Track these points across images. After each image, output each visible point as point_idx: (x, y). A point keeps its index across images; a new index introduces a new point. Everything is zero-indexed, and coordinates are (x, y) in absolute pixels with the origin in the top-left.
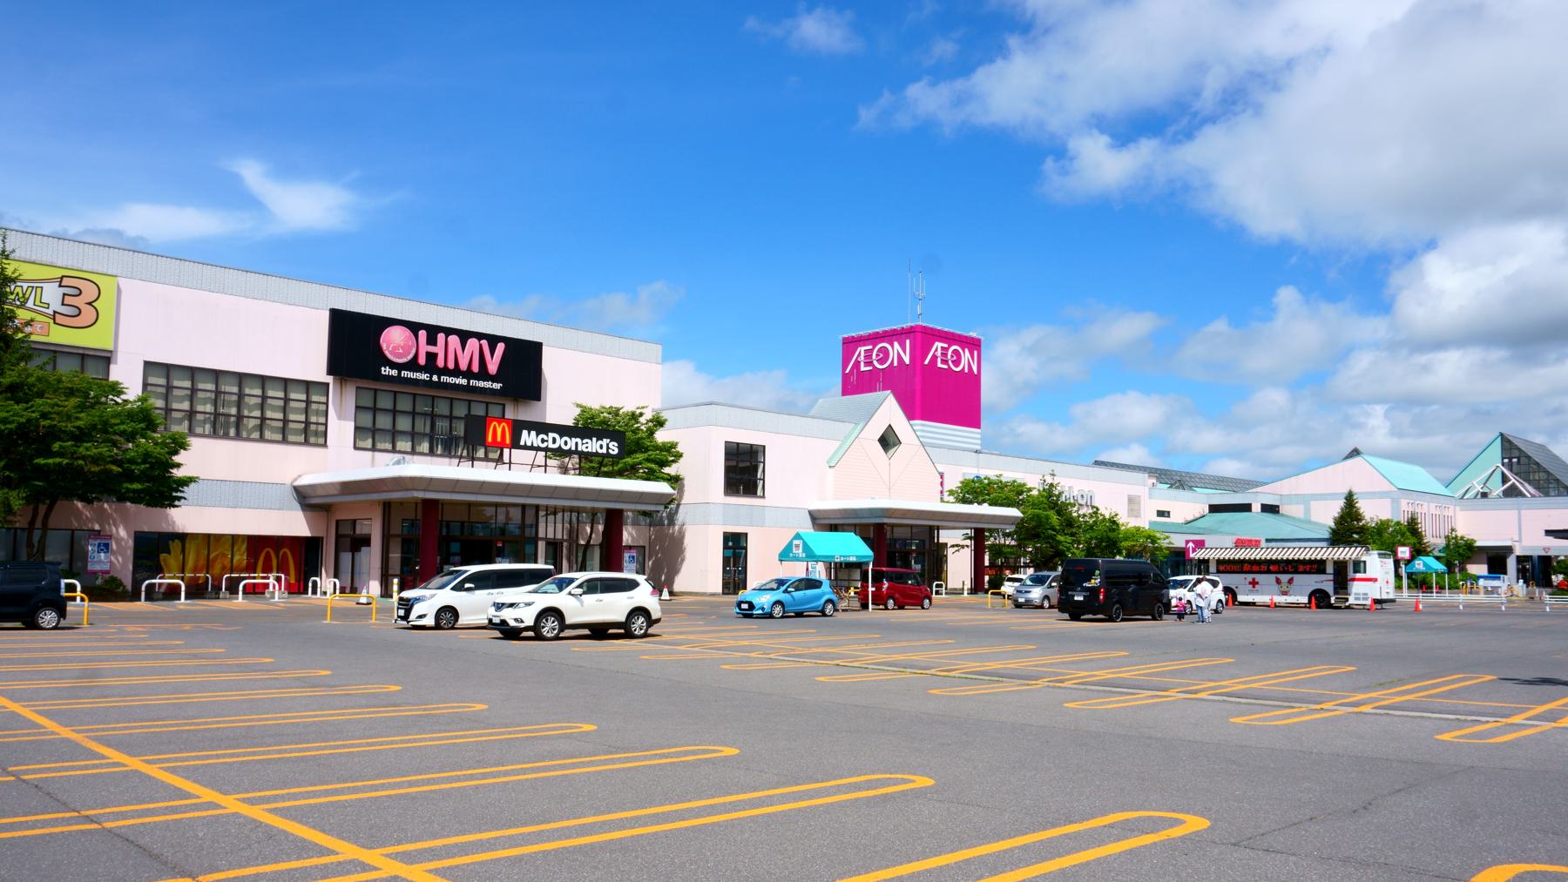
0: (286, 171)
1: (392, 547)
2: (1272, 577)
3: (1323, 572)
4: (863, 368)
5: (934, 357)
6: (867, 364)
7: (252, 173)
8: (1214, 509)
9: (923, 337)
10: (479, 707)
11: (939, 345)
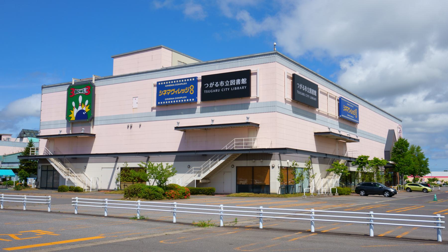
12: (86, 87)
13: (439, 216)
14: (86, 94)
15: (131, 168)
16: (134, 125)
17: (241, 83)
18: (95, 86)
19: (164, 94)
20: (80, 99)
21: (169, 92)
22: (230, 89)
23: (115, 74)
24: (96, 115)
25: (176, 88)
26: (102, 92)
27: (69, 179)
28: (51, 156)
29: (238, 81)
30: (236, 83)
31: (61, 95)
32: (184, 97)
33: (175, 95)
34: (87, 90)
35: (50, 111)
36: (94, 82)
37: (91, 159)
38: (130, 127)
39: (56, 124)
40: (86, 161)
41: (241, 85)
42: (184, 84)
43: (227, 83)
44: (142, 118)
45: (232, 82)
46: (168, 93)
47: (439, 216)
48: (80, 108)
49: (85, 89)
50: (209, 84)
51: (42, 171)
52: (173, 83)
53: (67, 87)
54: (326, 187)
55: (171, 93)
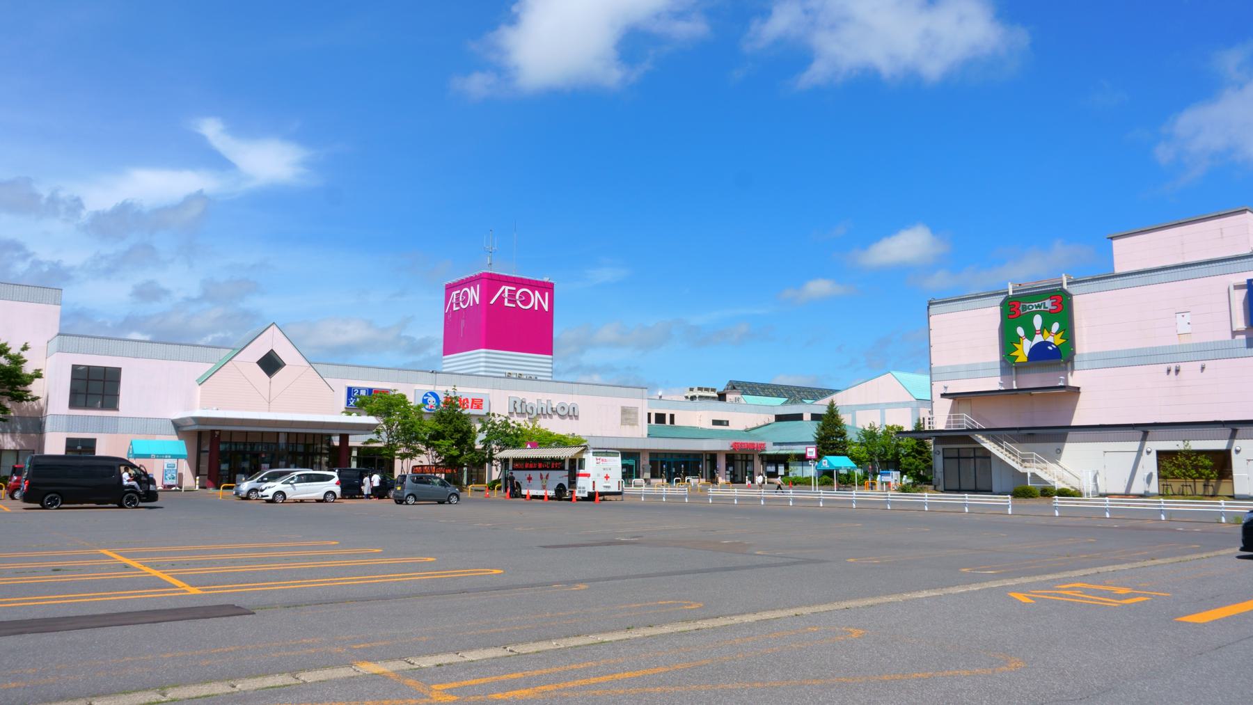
0: (242, 128)
1: (204, 442)
2: (538, 472)
3: (562, 469)
4: (506, 304)
5: (501, 298)
6: (510, 301)
7: (211, 129)
8: (779, 418)
9: (491, 282)
10: (496, 571)
11: (506, 288)
12: (1051, 298)
13: (1022, 598)
14: (1050, 311)
15: (1199, 453)
16: (1183, 366)
18: (1071, 296)
20: (1038, 321)
23: (1118, 271)
24: (1078, 351)
26: (1085, 304)
27: (1034, 475)
28: (980, 430)
31: (989, 316)
34: (1053, 304)
35: (967, 346)
36: (1065, 286)
37: (1071, 435)
38: (1173, 370)
39: (973, 371)
40: (1063, 439)
44: (1206, 353)
47: (1022, 598)
48: (1038, 339)
49: (1048, 303)
51: (944, 458)
53: (1001, 298)
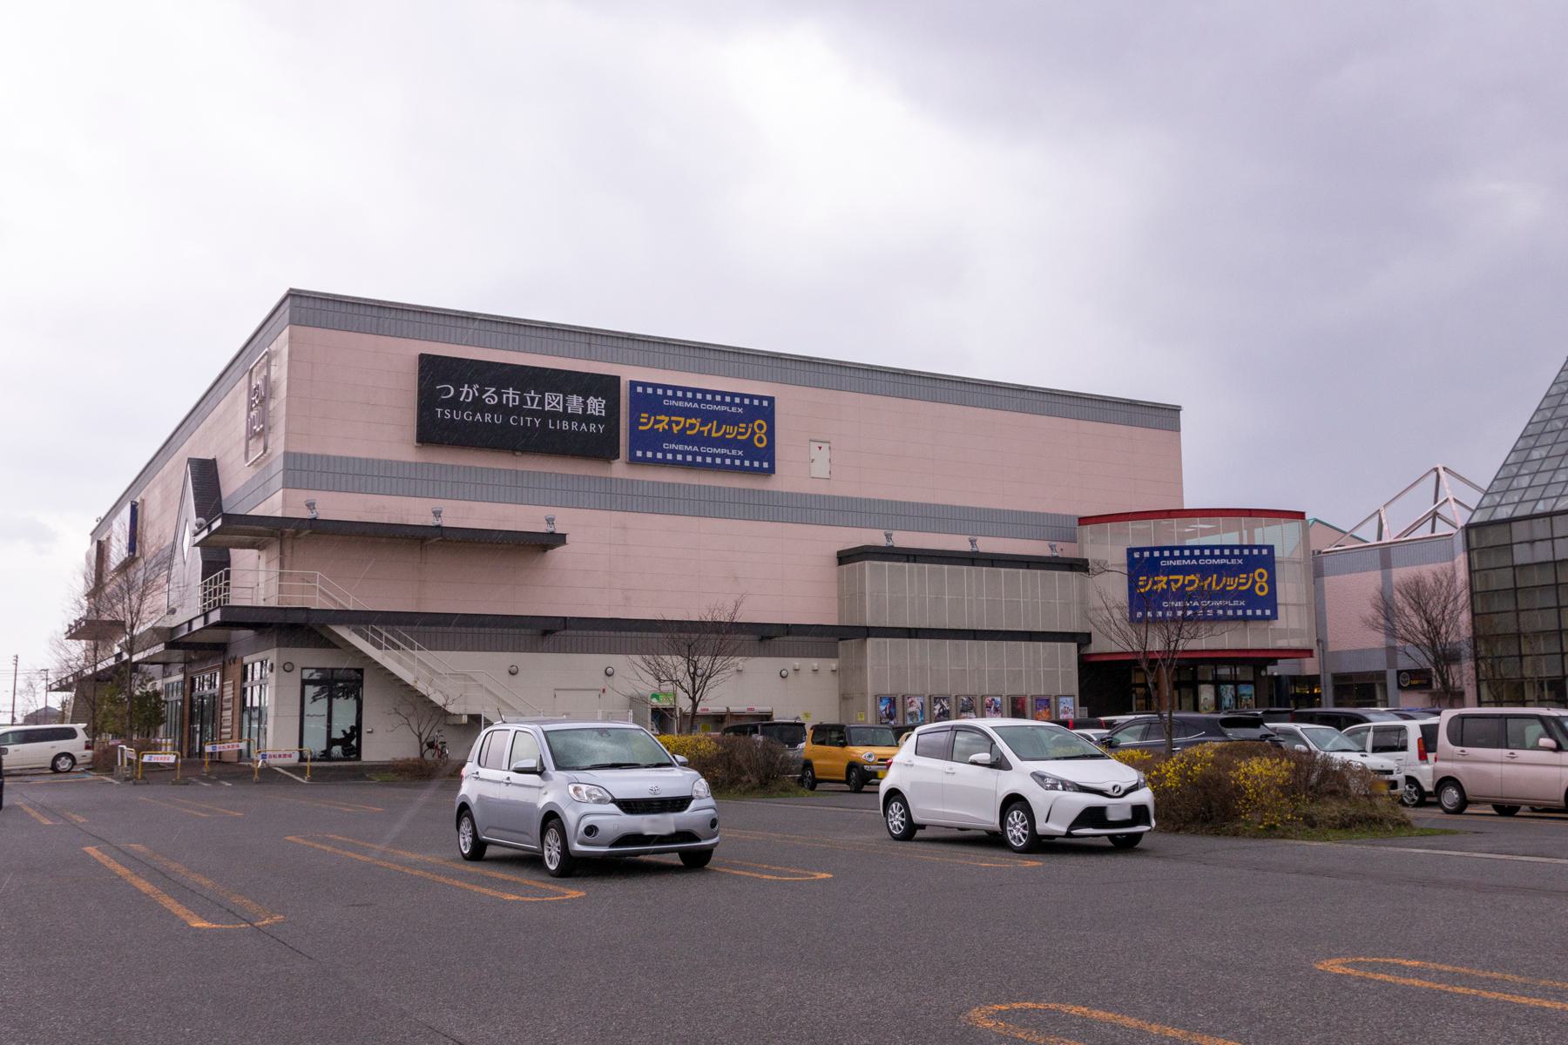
17: (585, 410)
19: (660, 426)
21: (678, 423)
22: (544, 424)
25: (707, 417)
29: (575, 403)
30: (565, 408)
32: (734, 452)
33: (700, 440)
41: (586, 418)
42: (734, 409)
43: (533, 399)
45: (553, 401)
46: (676, 429)
50: (458, 386)
52: (694, 400)
54: (1338, 756)
55: (684, 429)
